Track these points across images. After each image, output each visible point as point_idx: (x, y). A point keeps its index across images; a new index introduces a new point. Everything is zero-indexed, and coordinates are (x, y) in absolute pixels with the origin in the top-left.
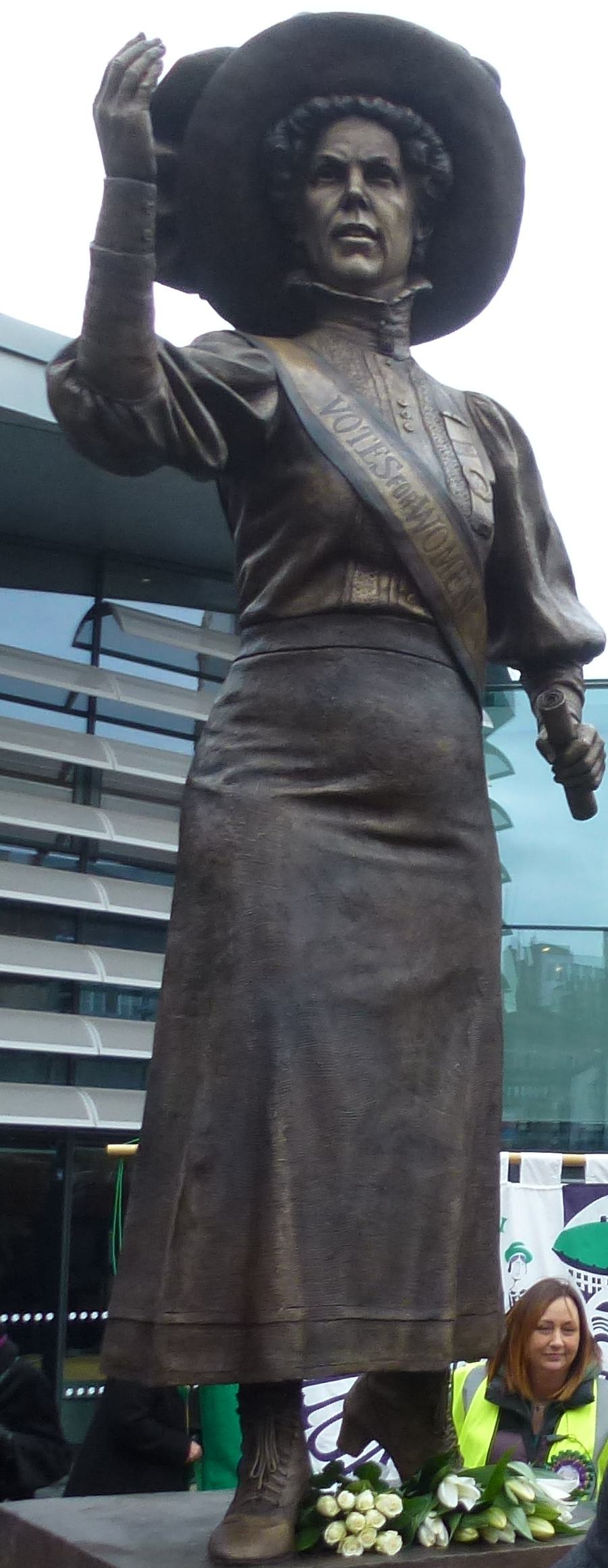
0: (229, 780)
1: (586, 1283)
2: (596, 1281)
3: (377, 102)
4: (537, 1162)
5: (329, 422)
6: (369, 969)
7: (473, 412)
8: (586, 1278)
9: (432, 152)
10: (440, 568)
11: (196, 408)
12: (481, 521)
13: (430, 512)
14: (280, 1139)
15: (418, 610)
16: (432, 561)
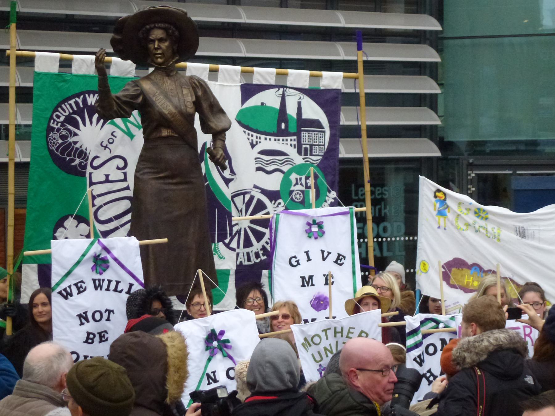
0: (141, 174)
1: (252, 138)
2: (258, 138)
3: (160, 25)
4: (226, 70)
5: (154, 99)
8: (252, 136)
9: (173, 32)
15: (176, 135)
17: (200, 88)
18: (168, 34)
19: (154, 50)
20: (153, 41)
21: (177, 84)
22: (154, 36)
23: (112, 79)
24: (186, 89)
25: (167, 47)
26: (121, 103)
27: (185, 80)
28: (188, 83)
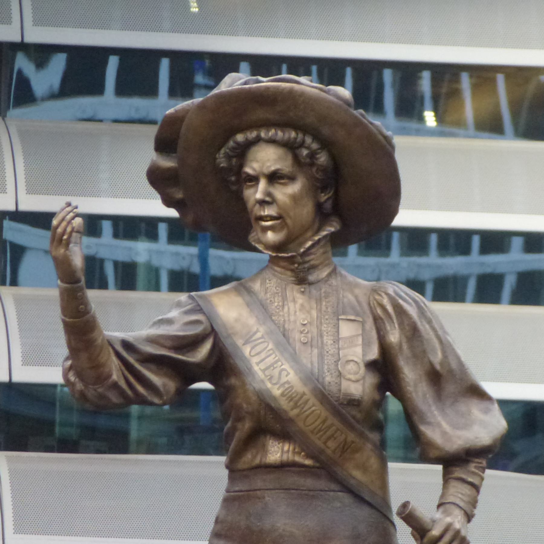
3: (272, 132)
7: (372, 305)
9: (312, 155)
10: (318, 435)
11: (139, 372)
12: (349, 397)
13: (307, 401)
16: (312, 432)
17: (395, 321)
19: (258, 206)
20: (254, 179)
21: (324, 308)
22: (256, 165)
24: (351, 324)
25: (295, 198)
26: (138, 360)
27: (356, 297)
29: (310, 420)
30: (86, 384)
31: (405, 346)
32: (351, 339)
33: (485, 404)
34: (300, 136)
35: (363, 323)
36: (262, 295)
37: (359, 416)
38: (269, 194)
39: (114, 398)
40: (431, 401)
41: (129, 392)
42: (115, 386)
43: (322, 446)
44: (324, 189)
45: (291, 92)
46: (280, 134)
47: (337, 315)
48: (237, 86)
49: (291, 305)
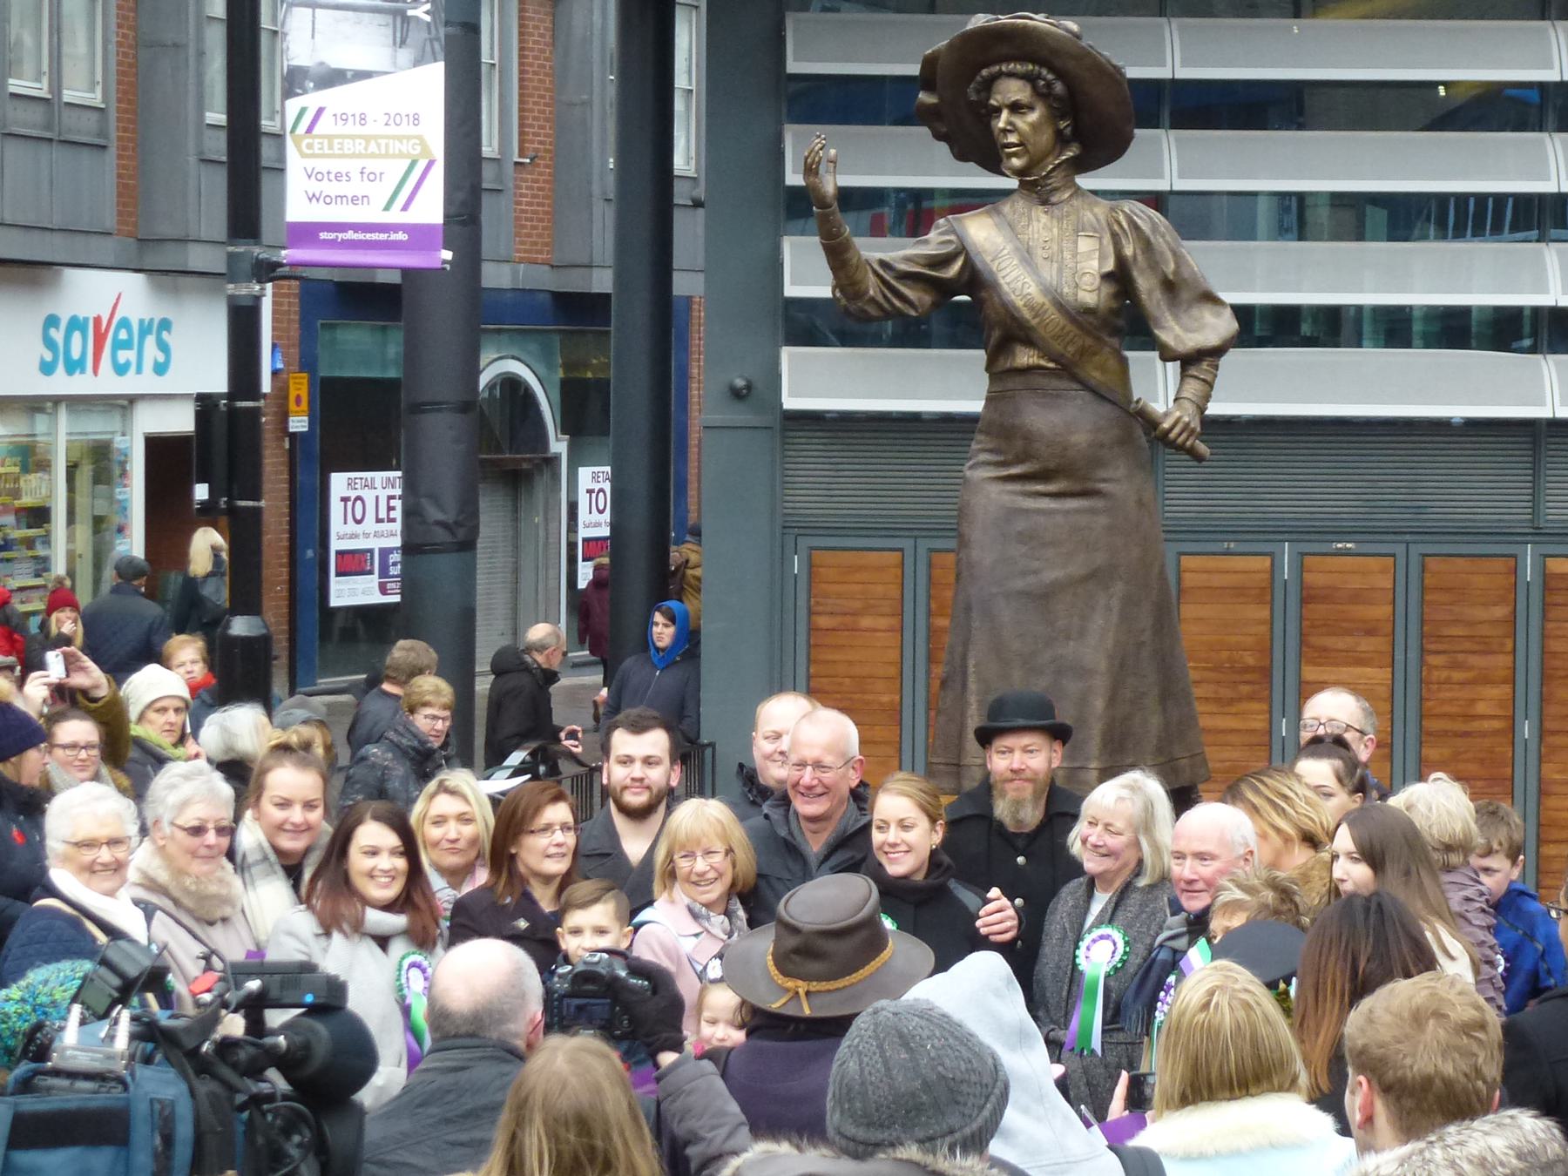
6: (1035, 572)
14: (971, 669)
15: (1051, 365)
18: (1036, 91)
20: (998, 110)
22: (999, 97)
23: (1180, 198)
24: (1088, 240)
27: (1095, 216)
28: (1104, 222)
29: (1050, 328)
30: (848, 299)
31: (1140, 258)
32: (1089, 255)
33: (1217, 308)
34: (1037, 68)
35: (1100, 239)
36: (1010, 217)
37: (1095, 322)
38: (1011, 123)
39: (873, 311)
40: (1164, 307)
41: (886, 305)
42: (873, 300)
43: (1062, 351)
44: (1062, 118)
45: (1025, 27)
46: (1018, 67)
47: (1076, 231)
48: (980, 24)
49: (1035, 223)
